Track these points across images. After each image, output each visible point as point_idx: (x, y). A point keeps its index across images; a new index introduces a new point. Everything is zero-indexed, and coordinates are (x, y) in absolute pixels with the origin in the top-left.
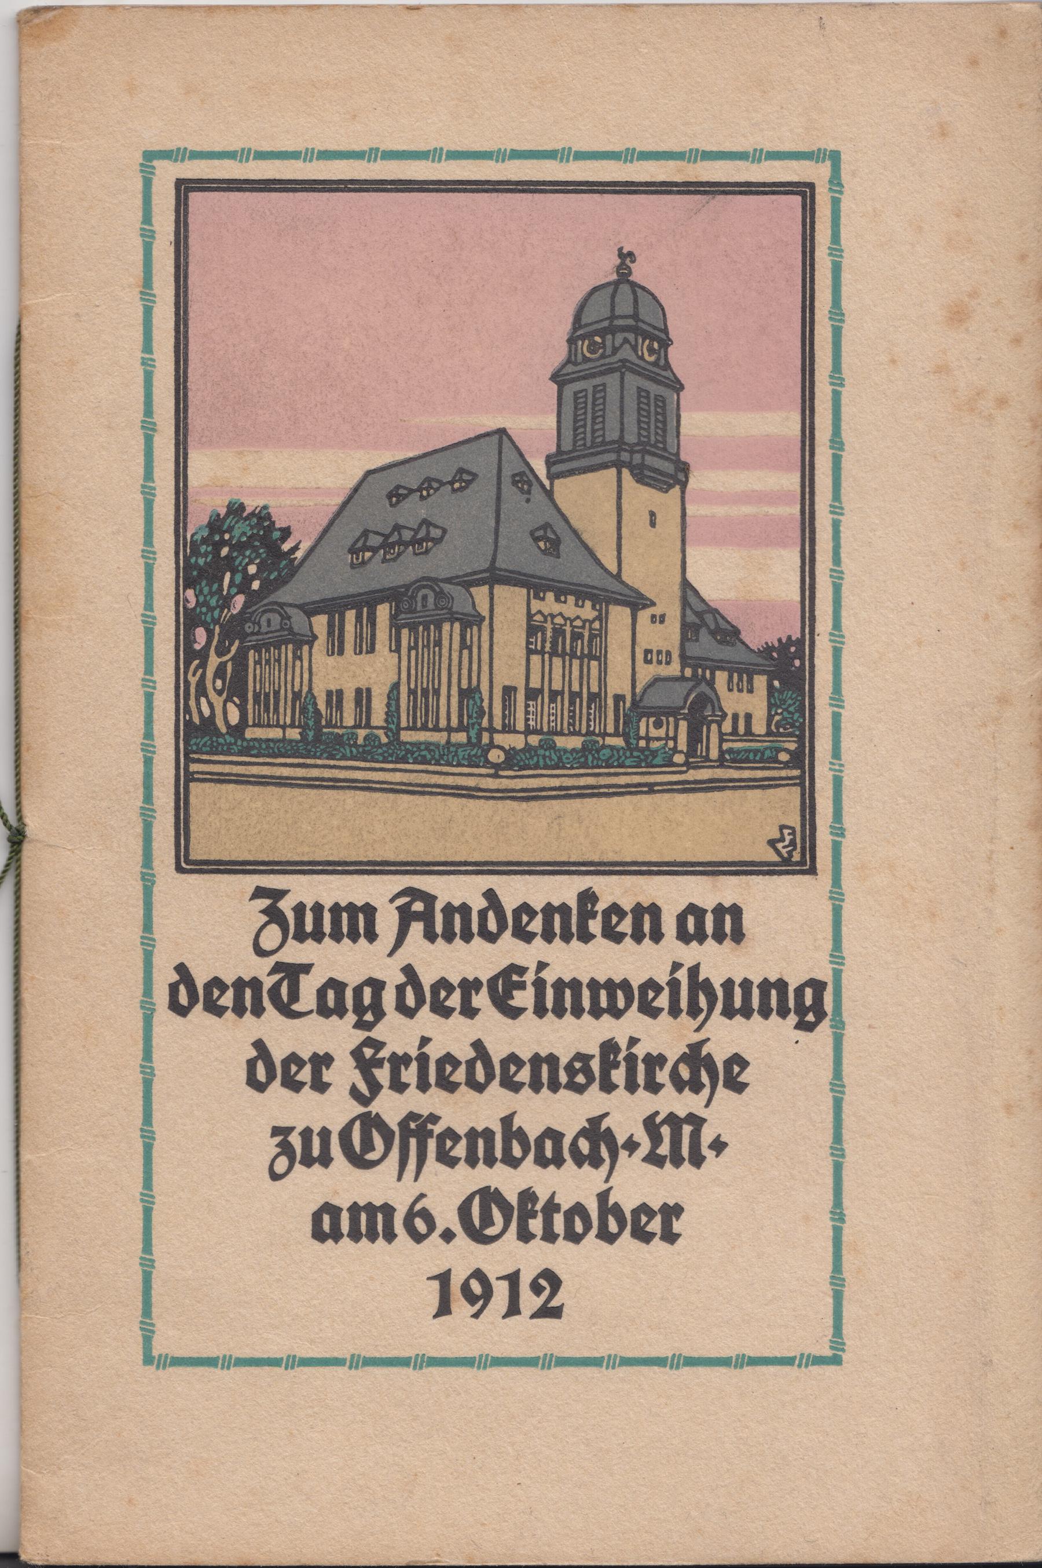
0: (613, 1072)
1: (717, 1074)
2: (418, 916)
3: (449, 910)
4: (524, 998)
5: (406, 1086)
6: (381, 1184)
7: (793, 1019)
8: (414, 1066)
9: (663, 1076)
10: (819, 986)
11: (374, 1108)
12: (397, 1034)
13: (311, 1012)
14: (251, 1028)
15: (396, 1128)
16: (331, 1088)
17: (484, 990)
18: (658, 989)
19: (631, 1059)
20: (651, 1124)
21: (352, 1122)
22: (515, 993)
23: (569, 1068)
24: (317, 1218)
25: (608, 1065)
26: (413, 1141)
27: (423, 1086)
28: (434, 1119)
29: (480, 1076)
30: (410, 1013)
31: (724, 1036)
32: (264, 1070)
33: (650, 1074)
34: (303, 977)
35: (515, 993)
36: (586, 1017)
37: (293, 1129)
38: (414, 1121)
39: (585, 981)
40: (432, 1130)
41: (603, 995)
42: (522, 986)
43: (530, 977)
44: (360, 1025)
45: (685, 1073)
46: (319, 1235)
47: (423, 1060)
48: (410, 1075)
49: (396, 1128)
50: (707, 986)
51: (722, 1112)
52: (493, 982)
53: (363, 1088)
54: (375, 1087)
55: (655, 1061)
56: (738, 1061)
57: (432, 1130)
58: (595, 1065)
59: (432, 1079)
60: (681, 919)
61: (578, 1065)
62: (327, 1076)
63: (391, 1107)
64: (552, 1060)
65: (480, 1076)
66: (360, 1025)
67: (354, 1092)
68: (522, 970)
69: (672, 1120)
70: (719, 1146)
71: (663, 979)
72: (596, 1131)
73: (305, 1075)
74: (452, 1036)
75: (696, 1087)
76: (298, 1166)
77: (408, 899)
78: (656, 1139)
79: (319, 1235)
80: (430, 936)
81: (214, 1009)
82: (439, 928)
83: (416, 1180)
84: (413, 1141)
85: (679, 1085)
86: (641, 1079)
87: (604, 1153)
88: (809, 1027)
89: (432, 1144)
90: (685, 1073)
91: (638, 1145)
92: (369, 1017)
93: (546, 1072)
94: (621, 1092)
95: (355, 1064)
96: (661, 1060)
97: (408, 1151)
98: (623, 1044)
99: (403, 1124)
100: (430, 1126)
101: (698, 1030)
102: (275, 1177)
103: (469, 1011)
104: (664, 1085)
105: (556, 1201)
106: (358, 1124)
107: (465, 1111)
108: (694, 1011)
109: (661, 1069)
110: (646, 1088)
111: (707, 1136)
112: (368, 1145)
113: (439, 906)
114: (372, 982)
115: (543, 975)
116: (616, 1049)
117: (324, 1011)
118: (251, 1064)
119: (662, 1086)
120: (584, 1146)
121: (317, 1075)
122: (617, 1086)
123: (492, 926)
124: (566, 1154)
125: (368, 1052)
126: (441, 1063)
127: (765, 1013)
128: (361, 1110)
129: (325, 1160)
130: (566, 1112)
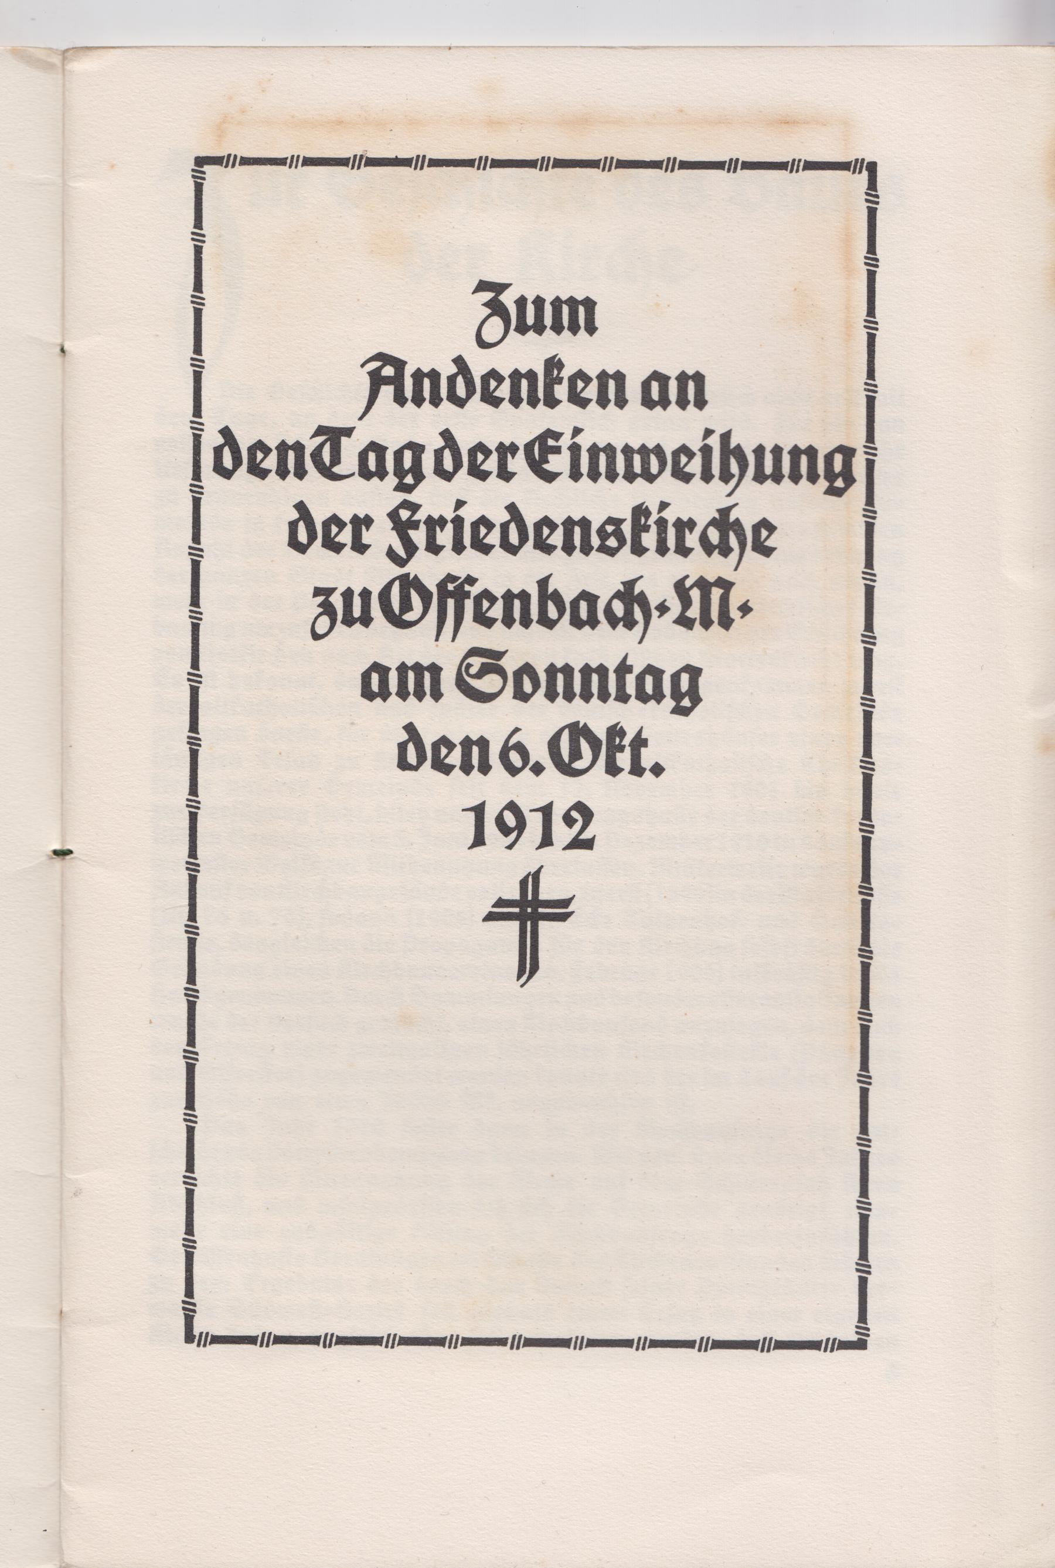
0: (644, 535)
1: (316, 533)
2: (387, 381)
3: (418, 376)
4: (559, 463)
5: (442, 548)
6: (417, 644)
7: (823, 484)
8: (450, 527)
9: (692, 540)
10: (848, 453)
11: (413, 568)
12: (434, 497)
13: (353, 474)
14: (293, 489)
15: (434, 590)
16: (775, 553)
17: (521, 454)
18: (691, 455)
19: (662, 523)
20: (681, 588)
21: (391, 583)
22: (551, 457)
23: (602, 533)
24: (366, 677)
25: (639, 529)
26: (451, 603)
27: (458, 547)
28: (471, 580)
29: (514, 538)
30: (448, 476)
31: (752, 502)
32: (306, 532)
33: (680, 539)
34: (344, 440)
35: (551, 457)
36: (620, 481)
37: (334, 590)
38: (452, 583)
39: (619, 447)
40: (469, 592)
41: (637, 459)
42: (557, 450)
43: (565, 442)
44: (401, 487)
45: (714, 535)
46: (368, 694)
47: (458, 522)
48: (445, 537)
49: (434, 590)
50: (739, 453)
51: (749, 576)
52: (529, 447)
53: (401, 552)
54: (411, 548)
55: (684, 526)
56: (766, 525)
57: (469, 592)
58: (627, 528)
59: (467, 540)
60: (646, 386)
61: (610, 529)
62: (366, 537)
63: (429, 569)
64: (585, 524)
65: (514, 538)
66: (401, 487)
67: (391, 554)
68: (557, 436)
69: (703, 585)
70: (745, 609)
71: (695, 446)
72: (629, 594)
73: (345, 537)
74: (486, 500)
75: (725, 550)
76: (339, 626)
77: (378, 364)
78: (686, 603)
79: (368, 694)
80: (400, 399)
81: (258, 472)
82: (408, 392)
83: (453, 640)
84: (451, 603)
85: (708, 548)
86: (671, 542)
87: (638, 614)
88: (838, 493)
89: (469, 605)
90: (714, 535)
91: (668, 609)
92: (409, 480)
93: (578, 536)
94: (652, 554)
95: (392, 525)
96: (691, 524)
97: (446, 614)
98: (654, 509)
99: (441, 586)
100: (467, 588)
101: (729, 495)
102: (316, 637)
103: (506, 475)
104: (692, 549)
105: (628, 663)
106: (397, 583)
107: (499, 572)
108: (726, 476)
109: (691, 531)
110: (677, 551)
111: (735, 600)
112: (406, 605)
113: (409, 371)
114: (412, 446)
115: (665, 514)
116: (647, 513)
117: (365, 474)
118: (293, 526)
119: (691, 550)
120: (618, 608)
121: (357, 536)
122: (647, 550)
123: (461, 391)
124: (601, 616)
125: (404, 514)
126: (475, 525)
127: (795, 477)
128: (399, 571)
129: (366, 620)
130: (599, 575)
